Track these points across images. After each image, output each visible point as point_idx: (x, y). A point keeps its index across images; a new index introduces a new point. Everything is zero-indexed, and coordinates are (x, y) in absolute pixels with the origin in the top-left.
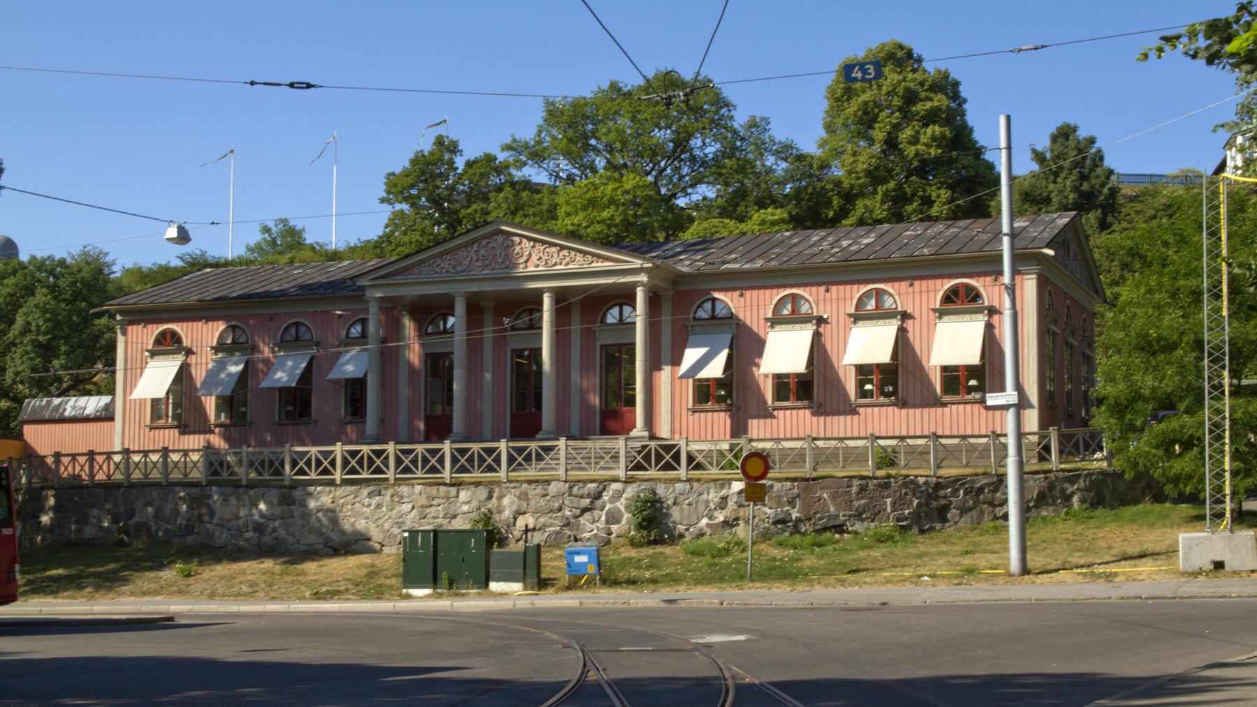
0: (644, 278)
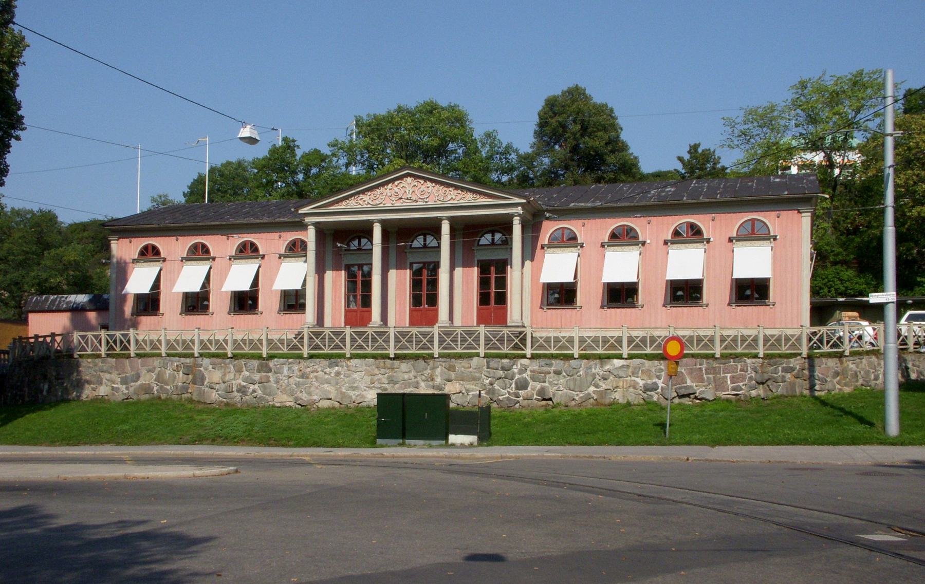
0: (519, 210)
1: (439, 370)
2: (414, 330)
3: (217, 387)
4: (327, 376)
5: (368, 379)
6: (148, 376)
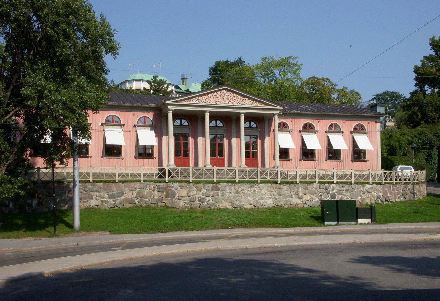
1: (300, 189)
2: (180, 168)
3: (184, 199)
4: (249, 192)
5: (268, 194)
6: (130, 194)
